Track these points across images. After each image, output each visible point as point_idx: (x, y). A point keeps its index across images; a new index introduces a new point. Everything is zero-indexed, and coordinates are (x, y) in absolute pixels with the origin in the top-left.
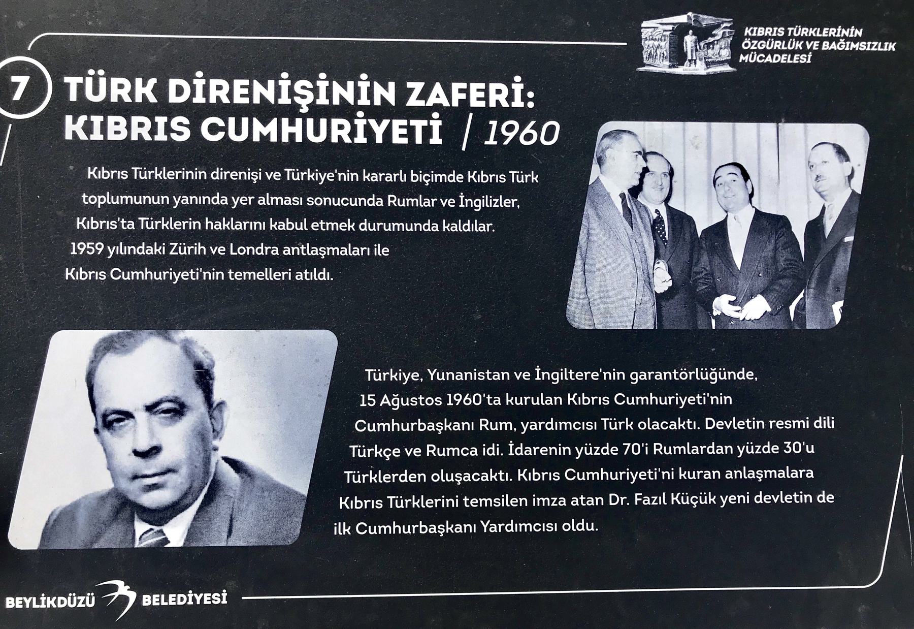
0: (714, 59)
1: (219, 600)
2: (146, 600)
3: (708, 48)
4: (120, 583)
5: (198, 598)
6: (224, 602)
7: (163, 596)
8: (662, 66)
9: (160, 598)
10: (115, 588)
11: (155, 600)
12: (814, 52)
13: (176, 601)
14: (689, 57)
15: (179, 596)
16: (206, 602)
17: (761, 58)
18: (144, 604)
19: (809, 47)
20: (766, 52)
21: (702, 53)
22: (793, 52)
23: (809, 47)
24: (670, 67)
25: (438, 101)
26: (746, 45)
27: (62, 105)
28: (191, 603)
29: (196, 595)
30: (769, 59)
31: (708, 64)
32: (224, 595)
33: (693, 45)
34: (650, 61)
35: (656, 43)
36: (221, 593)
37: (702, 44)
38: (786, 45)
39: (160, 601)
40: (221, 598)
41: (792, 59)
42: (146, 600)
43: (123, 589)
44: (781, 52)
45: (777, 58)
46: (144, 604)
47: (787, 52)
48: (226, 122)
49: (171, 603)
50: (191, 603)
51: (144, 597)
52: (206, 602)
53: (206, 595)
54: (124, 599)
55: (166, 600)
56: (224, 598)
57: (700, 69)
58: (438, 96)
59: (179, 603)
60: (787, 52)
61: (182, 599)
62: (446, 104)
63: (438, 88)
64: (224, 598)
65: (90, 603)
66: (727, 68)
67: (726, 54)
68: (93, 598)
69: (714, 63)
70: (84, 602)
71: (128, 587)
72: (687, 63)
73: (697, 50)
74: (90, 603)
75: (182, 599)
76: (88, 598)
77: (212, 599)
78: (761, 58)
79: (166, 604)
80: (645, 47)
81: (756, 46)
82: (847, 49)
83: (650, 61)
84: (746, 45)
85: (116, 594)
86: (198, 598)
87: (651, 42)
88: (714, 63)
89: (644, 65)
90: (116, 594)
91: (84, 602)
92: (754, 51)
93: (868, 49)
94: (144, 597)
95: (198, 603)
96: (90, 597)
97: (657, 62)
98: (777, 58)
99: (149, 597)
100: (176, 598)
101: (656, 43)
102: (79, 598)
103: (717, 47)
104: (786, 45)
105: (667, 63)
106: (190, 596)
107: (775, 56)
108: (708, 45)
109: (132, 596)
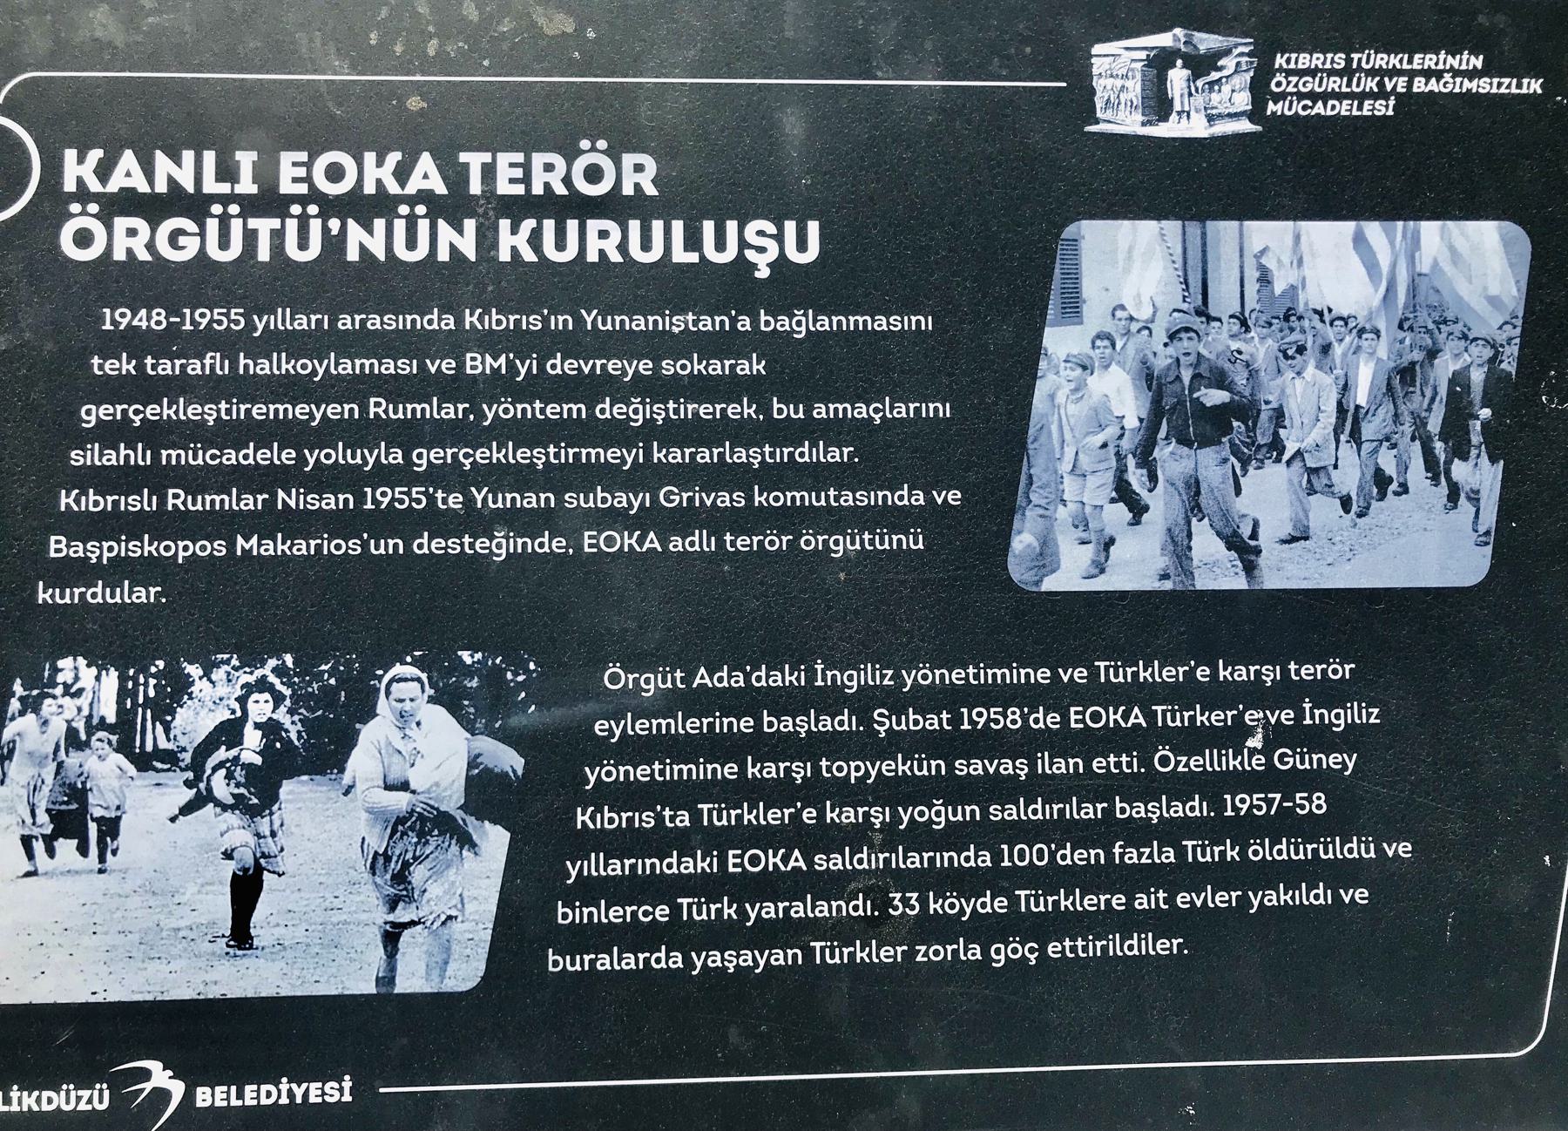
1: (337, 1094)
2: (203, 1097)
3: (1211, 90)
4: (155, 1066)
5: (299, 1092)
6: (347, 1098)
7: (233, 1088)
8: (1129, 122)
9: (228, 1092)
10: (146, 1075)
12: (1399, 96)
13: (258, 1098)
14: (1177, 107)
15: (264, 1088)
16: (313, 1099)
17: (1305, 108)
18: (199, 1104)
20: (1313, 97)
21: (1199, 100)
22: (1362, 97)
24: (1143, 124)
25: (128, 183)
26: (1279, 84)
28: (284, 1100)
29: (294, 1086)
30: (1319, 108)
31: (1211, 119)
32: (347, 1084)
33: (1185, 85)
34: (1108, 115)
35: (1119, 83)
36: (340, 1081)
37: (1200, 83)
38: (1349, 85)
39: (228, 1099)
40: (341, 1090)
41: (1360, 108)
42: (203, 1097)
43: (160, 1076)
44: (1340, 96)
45: (1333, 107)
46: (199, 1104)
47: (1351, 96)
48: (781, 229)
49: (249, 1102)
50: (284, 1100)
51: (199, 1090)
52: (313, 1099)
53: (313, 1086)
54: (162, 1095)
55: (240, 1096)
56: (347, 1091)
57: (1197, 128)
58: (128, 174)
59: (264, 1101)
60: (1351, 96)
61: (269, 1094)
62: (143, 187)
63: (128, 159)
66: (1245, 126)
67: (1243, 101)
68: (106, 1093)
70: (90, 1101)
71: (170, 1073)
72: (1174, 117)
73: (1190, 94)
74: (101, 1102)
75: (269, 1094)
76: (96, 1093)
77: (324, 1094)
78: (1305, 108)
79: (240, 1103)
81: (1296, 86)
82: (1457, 90)
83: (1108, 115)
84: (1279, 84)
85: (148, 1087)
86: (299, 1092)
87: (1109, 82)
88: (1220, 116)
89: (1097, 122)
90: (148, 1087)
91: (90, 1101)
92: (1292, 94)
93: (1494, 90)
94: (199, 1090)
96: (101, 1090)
97: (1121, 116)
98: (1333, 107)
99: (208, 1090)
100: (258, 1091)
101: (1119, 83)
102: (80, 1093)
103: (1226, 89)
104: (1349, 85)
105: (1139, 118)
106: (284, 1087)
107: (1330, 103)
108: (1211, 84)
109: (178, 1089)
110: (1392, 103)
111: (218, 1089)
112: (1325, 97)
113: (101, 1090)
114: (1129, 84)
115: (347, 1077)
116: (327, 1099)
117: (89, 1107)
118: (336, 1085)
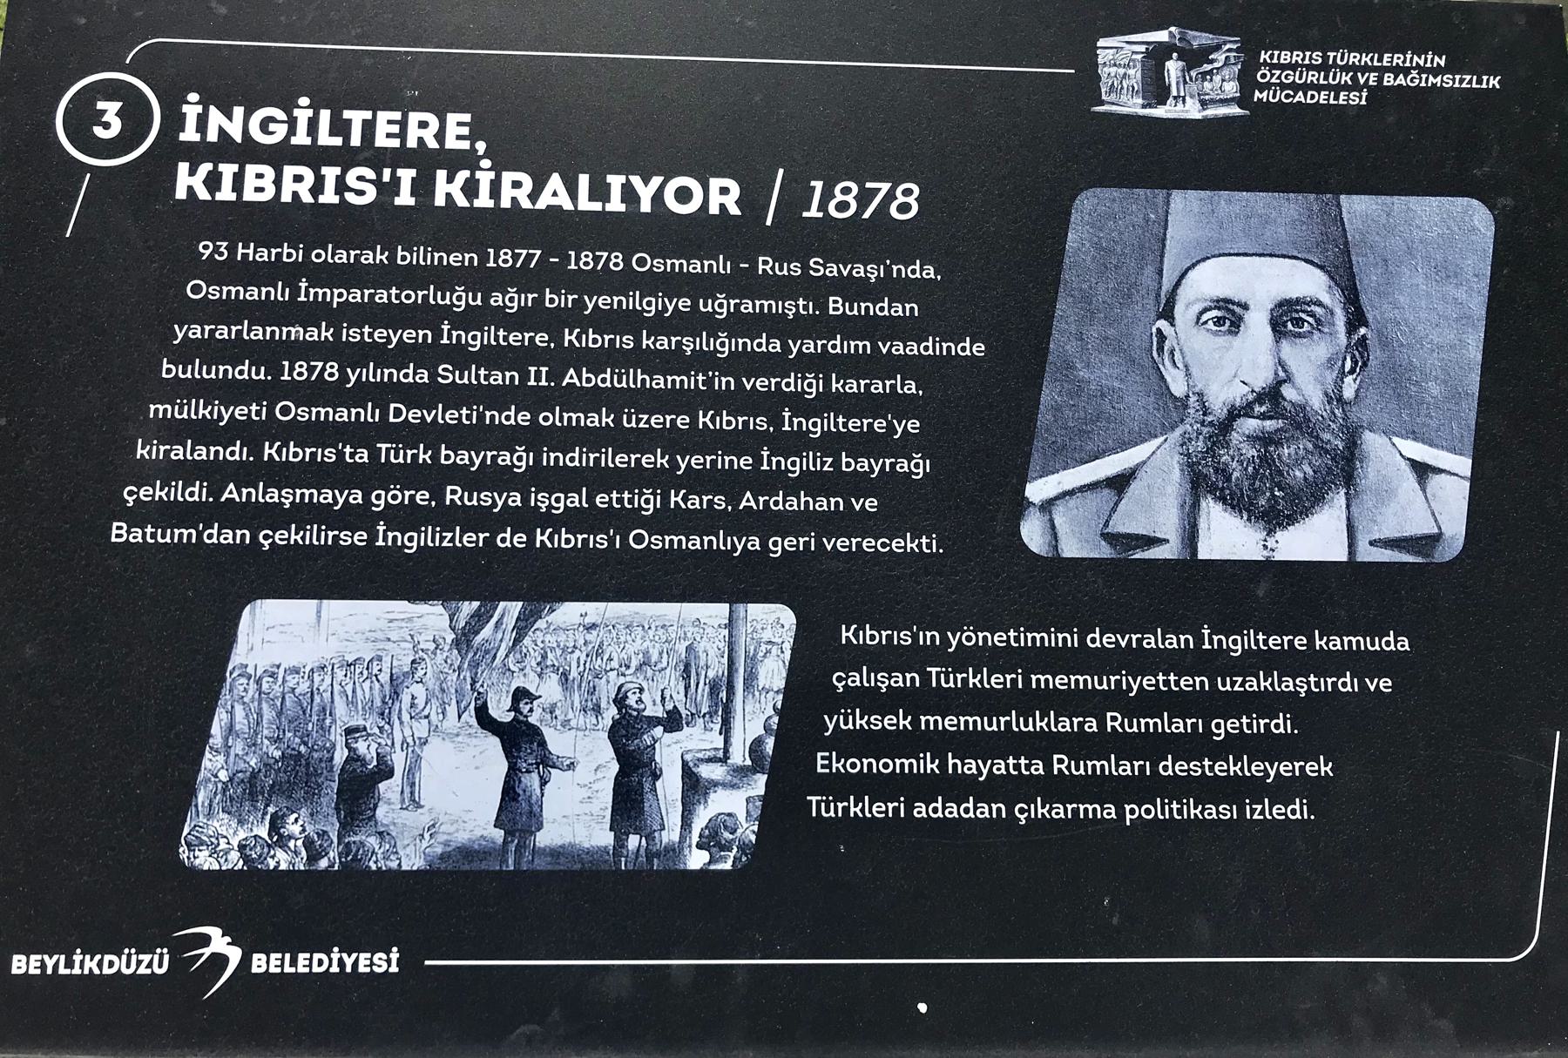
0: (1213, 96)
1: (385, 965)
2: (259, 963)
3: (1204, 80)
4: (214, 932)
5: (349, 962)
7: (288, 956)
8: (1133, 105)
9: (283, 960)
10: (205, 940)
11: (273, 962)
12: (1370, 88)
13: (310, 966)
15: (317, 956)
17: (1287, 96)
18: (255, 970)
19: (1362, 81)
20: (1295, 87)
22: (1337, 89)
23: (1362, 81)
24: (1144, 106)
26: (1264, 76)
27: (171, 151)
28: (335, 969)
29: (345, 956)
30: (1300, 97)
31: (1204, 104)
32: (395, 956)
34: (1113, 98)
35: (1122, 71)
36: (388, 952)
37: (1193, 74)
38: (1326, 78)
39: (282, 966)
40: (389, 961)
41: (1336, 98)
42: (259, 963)
43: (219, 943)
45: (1313, 97)
46: (255, 970)
47: (1328, 87)
49: (301, 970)
50: (335, 969)
51: (256, 956)
53: (363, 956)
54: (220, 960)
55: (294, 963)
56: (394, 962)
59: (316, 969)
60: (1328, 87)
61: (320, 963)
64: (394, 962)
65: (160, 966)
66: (1235, 110)
67: (1231, 88)
68: (166, 958)
69: (1213, 101)
70: (150, 965)
71: (228, 939)
72: (1171, 101)
73: (1185, 82)
74: (160, 966)
75: (320, 963)
76: (156, 958)
78: (1287, 96)
79: (293, 970)
80: (1104, 77)
83: (1113, 98)
85: (207, 952)
86: (349, 962)
87: (1113, 70)
88: (1213, 101)
89: (1102, 103)
90: (207, 952)
91: (150, 965)
94: (256, 956)
95: (348, 969)
96: (161, 955)
98: (1313, 97)
100: (311, 959)
101: (1122, 71)
102: (141, 957)
103: (1217, 78)
104: (1326, 78)
105: (1140, 101)
106: (335, 956)
108: (1204, 74)
109: (235, 955)
110: (1364, 94)
111: (273, 956)
112: (1305, 88)
113: (161, 955)
114: (1131, 72)
115: (395, 949)
116: (376, 969)
117: (149, 971)
118: (384, 956)
